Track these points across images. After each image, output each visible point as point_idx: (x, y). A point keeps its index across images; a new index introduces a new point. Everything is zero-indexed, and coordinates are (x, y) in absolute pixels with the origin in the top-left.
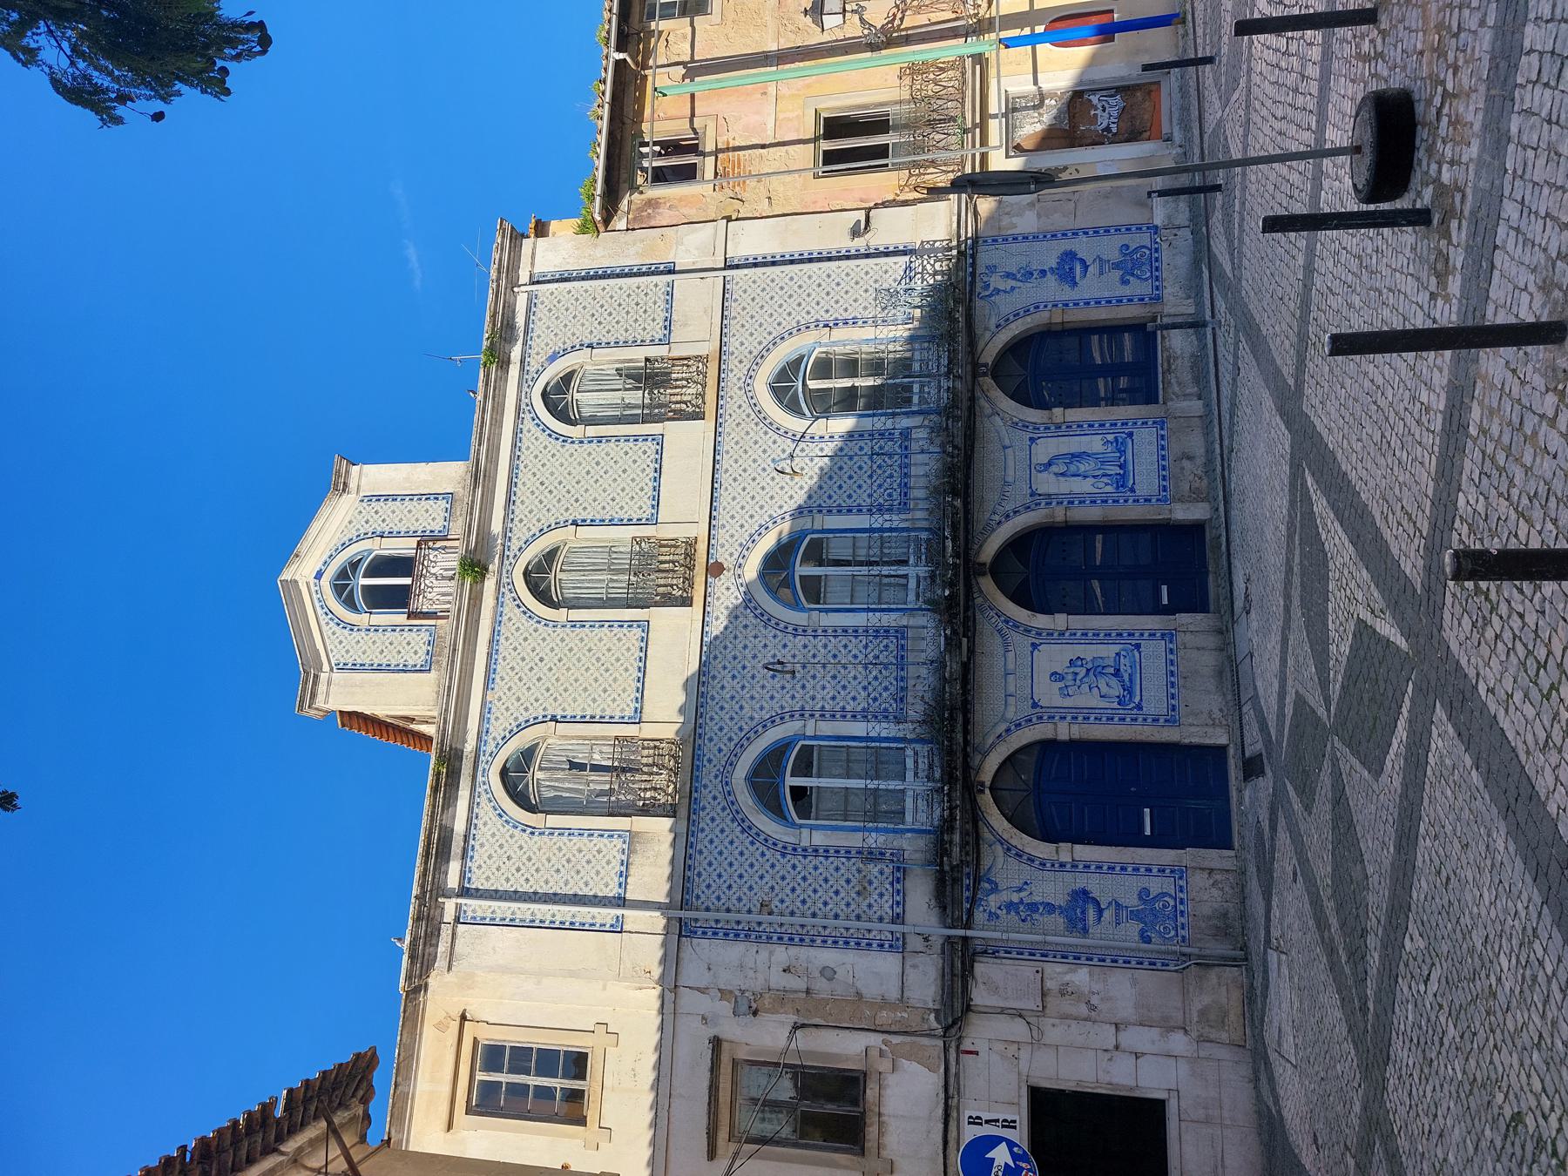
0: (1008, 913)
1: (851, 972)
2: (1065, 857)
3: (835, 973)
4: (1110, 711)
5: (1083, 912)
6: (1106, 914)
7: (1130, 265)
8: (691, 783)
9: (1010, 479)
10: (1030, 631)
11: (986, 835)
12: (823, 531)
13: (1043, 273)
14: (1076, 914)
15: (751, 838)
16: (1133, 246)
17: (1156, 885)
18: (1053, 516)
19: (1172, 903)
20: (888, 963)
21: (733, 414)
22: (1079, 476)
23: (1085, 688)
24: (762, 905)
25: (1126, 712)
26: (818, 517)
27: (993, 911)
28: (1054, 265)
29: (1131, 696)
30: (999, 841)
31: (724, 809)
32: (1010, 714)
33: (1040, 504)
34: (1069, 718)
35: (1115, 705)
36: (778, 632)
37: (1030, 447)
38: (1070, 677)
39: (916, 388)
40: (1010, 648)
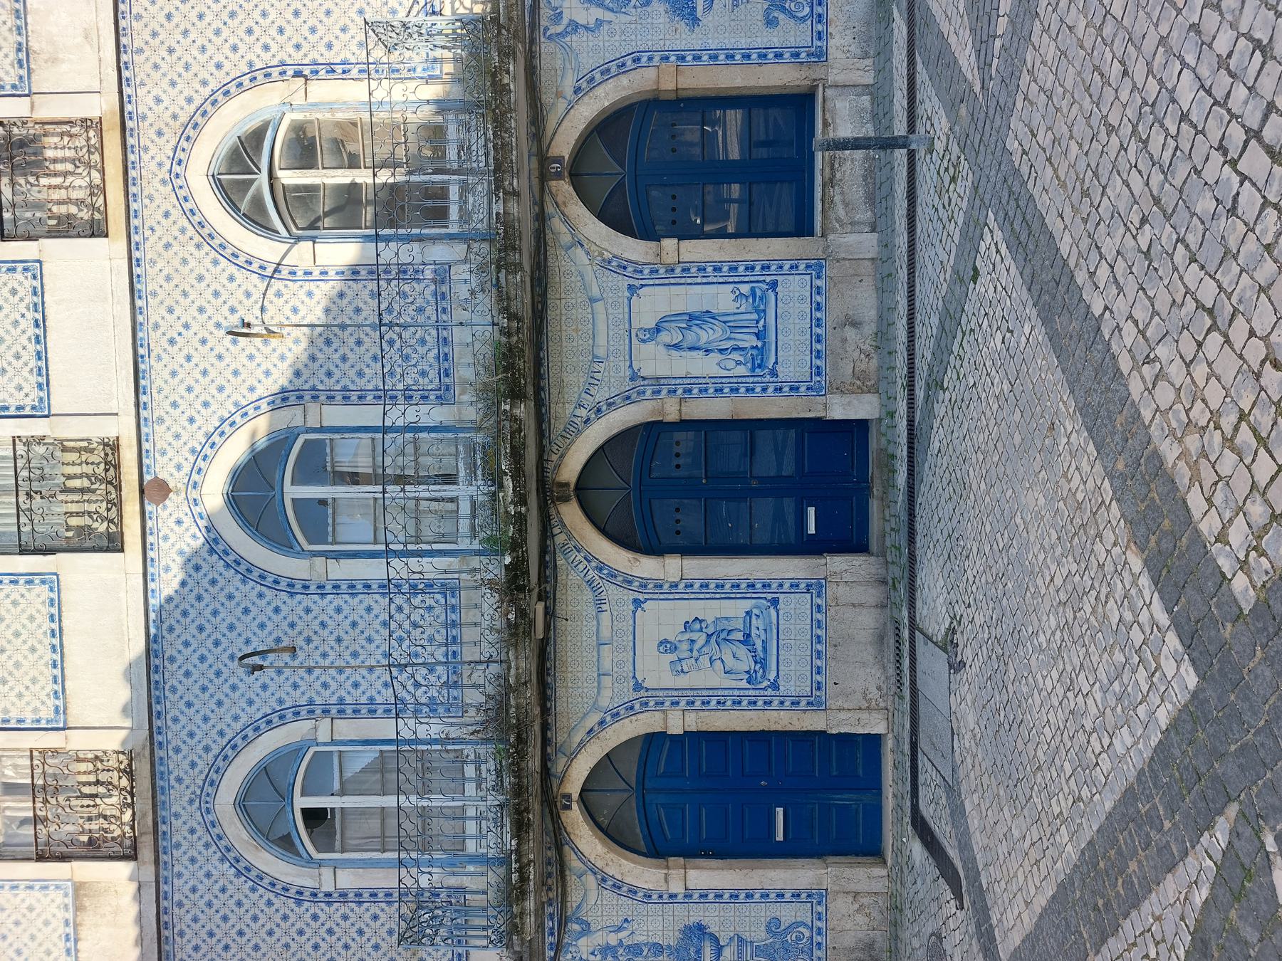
2: (677, 887)
4: (736, 692)
6: (727, 953)
9: (601, 352)
11: (574, 863)
12: (322, 429)
15: (251, 883)
17: (788, 913)
18: (662, 412)
19: (807, 934)
21: (156, 227)
23: (705, 660)
25: (757, 693)
26: (313, 408)
31: (207, 846)
32: (605, 702)
34: (683, 703)
35: (744, 684)
38: (685, 646)
39: (454, 192)
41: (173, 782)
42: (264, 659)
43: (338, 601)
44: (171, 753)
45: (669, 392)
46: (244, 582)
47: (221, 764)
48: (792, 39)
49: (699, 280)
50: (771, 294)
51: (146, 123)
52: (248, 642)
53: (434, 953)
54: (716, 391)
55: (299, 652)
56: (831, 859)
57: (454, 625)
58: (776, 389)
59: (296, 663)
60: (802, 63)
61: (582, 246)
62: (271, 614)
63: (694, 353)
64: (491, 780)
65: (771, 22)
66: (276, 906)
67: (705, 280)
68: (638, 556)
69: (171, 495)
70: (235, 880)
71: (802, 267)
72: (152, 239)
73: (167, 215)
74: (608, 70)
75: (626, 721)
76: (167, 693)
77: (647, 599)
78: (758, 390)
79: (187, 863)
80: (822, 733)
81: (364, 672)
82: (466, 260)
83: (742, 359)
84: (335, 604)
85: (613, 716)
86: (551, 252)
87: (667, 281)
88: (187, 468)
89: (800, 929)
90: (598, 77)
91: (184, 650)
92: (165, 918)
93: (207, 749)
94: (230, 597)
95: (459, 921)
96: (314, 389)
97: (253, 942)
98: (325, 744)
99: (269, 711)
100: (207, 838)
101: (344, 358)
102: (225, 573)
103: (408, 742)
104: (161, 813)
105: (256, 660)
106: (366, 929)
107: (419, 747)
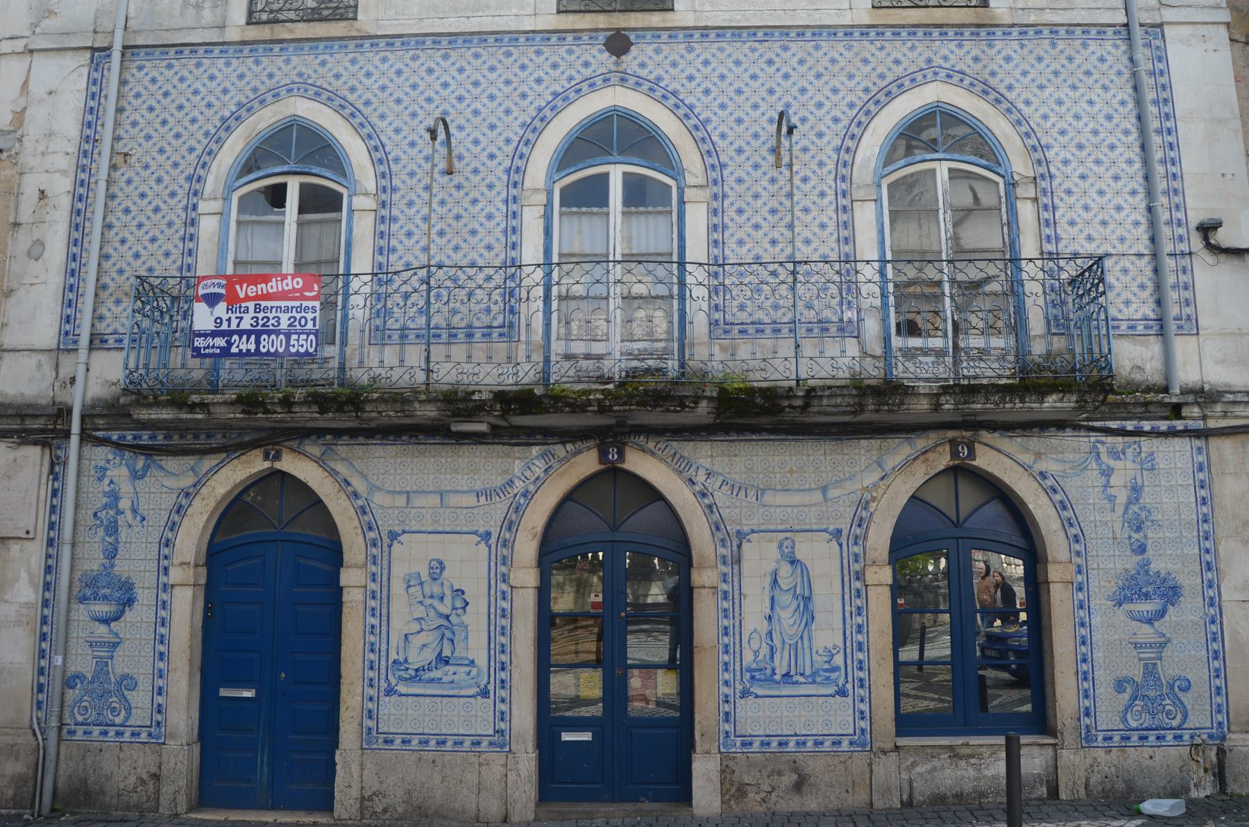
0: (105, 494)
1: (35, 281)
2: (175, 575)
3: (37, 260)
4: (384, 647)
5: (105, 597)
6: (102, 629)
7: (1152, 694)
8: (293, 40)
9: (768, 498)
10: (509, 529)
11: (208, 462)
12: (682, 203)
13: (1142, 549)
14: (104, 587)
15: (213, 131)
16: (1187, 698)
17: (140, 699)
18: (701, 567)
19: (118, 720)
20: (45, 332)
21: (884, 53)
22: (772, 608)
23: (420, 612)
24: (126, 155)
25: (383, 671)
26: (704, 194)
27: (108, 473)
28: (1154, 567)
29: (406, 679)
30: (199, 482)
31: (255, 90)
32: (378, 499)
33: (724, 546)
34: (373, 586)
35: (393, 656)
36: (515, 144)
37: (825, 531)
38: (436, 590)
39: (936, 343)
40: (482, 500)
41: (321, 58)
42: (442, 143)
43: (499, 217)
44: (352, 55)
45: (725, 575)
46: (523, 125)
47: (336, 103)
48: (1103, 708)
49: (847, 608)
50: (831, 690)
51: (985, 48)
52: (461, 128)
53: (125, 314)
54: (726, 628)
55: (447, 178)
56: (197, 749)
57: (470, 335)
58: (727, 696)
59: (436, 176)
60: (1079, 719)
61: (882, 478)
62: (488, 151)
63: (767, 603)
64: (301, 374)
65: (1120, 685)
66: (188, 156)
67: (847, 615)
68: (539, 538)
69: (614, 58)
70: (218, 117)
71: (863, 724)
72: (872, 48)
73: (897, 62)
74: (1064, 508)
75: (357, 522)
76: (412, 52)
77: (490, 547)
78: (726, 676)
79: (239, 72)
80: (335, 744)
81: (424, 242)
82: (865, 354)
83: (761, 657)
84: (497, 214)
85: (362, 508)
86: (875, 443)
87: (846, 572)
88: (643, 73)
89: (123, 713)
90: (1058, 497)
91: (455, 67)
92: (187, 50)
93: (353, 89)
94: (508, 112)
95: (156, 340)
96: (724, 196)
97: (154, 134)
98: (350, 204)
99: (387, 149)
100: (263, 89)
101: (757, 227)
102: (533, 107)
103: (347, 285)
104: (292, 46)
105: (441, 136)
106: (156, 245)
107: (340, 298)
